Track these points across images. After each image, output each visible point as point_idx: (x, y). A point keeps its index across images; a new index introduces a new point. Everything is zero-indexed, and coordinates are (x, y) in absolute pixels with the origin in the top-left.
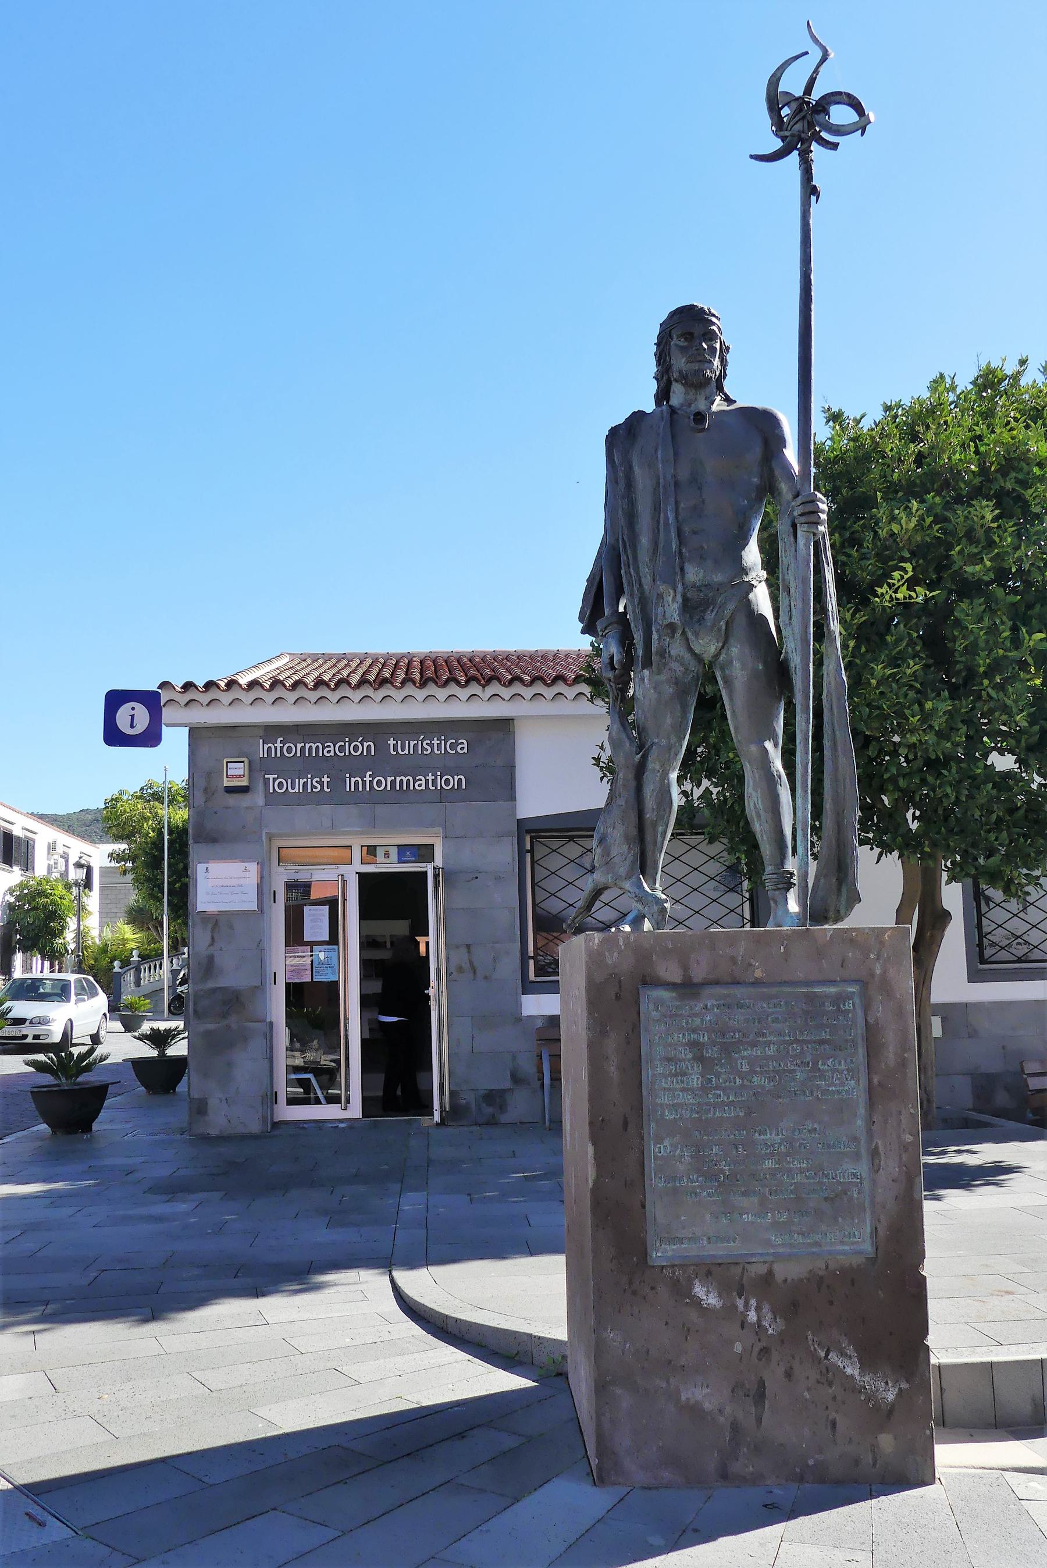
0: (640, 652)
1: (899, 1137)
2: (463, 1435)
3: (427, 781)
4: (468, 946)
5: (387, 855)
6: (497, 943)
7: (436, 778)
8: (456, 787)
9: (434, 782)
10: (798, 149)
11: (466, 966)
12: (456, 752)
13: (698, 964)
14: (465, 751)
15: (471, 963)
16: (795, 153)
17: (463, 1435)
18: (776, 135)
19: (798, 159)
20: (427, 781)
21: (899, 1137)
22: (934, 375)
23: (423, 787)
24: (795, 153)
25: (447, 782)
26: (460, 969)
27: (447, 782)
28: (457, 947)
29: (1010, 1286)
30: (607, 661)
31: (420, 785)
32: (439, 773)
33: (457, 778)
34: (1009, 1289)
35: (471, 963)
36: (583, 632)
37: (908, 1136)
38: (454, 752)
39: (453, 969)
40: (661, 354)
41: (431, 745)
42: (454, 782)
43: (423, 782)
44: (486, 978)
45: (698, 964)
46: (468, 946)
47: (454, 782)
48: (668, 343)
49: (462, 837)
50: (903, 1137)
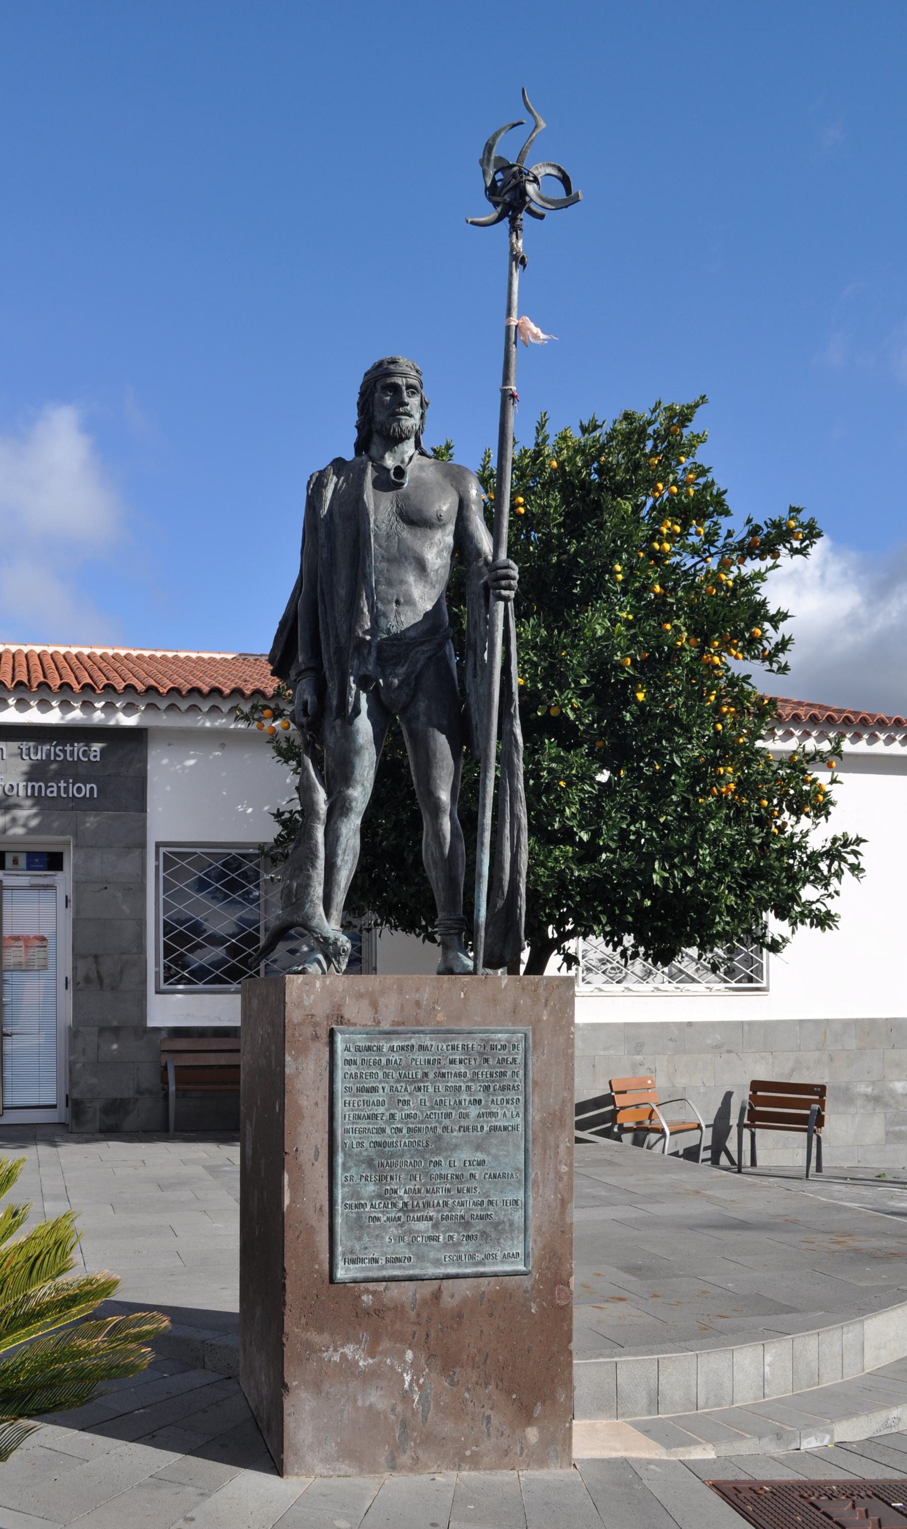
0: (335, 702)
1: (556, 1168)
2: (155, 1434)
3: (59, 788)
4: (96, 957)
5: (15, 862)
6: (124, 953)
7: (68, 786)
8: (88, 796)
9: (66, 790)
10: (509, 216)
11: (94, 976)
12: (89, 759)
13: (387, 1006)
14: (98, 759)
15: (98, 972)
16: (507, 219)
17: (155, 1434)
18: (490, 200)
19: (508, 225)
20: (59, 788)
21: (556, 1168)
22: (386, 356)
23: (55, 794)
24: (507, 219)
25: (79, 790)
26: (87, 979)
27: (79, 790)
28: (85, 957)
29: (623, 1294)
30: (300, 708)
31: (52, 792)
32: (71, 781)
33: (88, 786)
34: (621, 1296)
35: (98, 972)
36: (273, 673)
37: (564, 1166)
38: (86, 759)
39: (80, 978)
40: (364, 404)
41: (64, 751)
42: (86, 790)
43: (55, 789)
44: (113, 989)
45: (387, 1006)
46: (96, 957)
47: (86, 790)
48: (372, 394)
49: (91, 847)
50: (559, 1167)
